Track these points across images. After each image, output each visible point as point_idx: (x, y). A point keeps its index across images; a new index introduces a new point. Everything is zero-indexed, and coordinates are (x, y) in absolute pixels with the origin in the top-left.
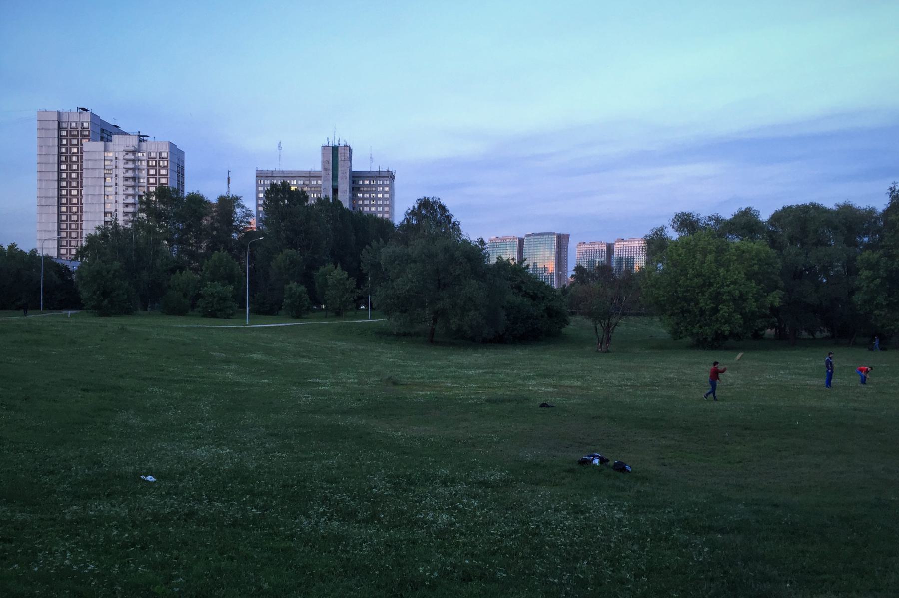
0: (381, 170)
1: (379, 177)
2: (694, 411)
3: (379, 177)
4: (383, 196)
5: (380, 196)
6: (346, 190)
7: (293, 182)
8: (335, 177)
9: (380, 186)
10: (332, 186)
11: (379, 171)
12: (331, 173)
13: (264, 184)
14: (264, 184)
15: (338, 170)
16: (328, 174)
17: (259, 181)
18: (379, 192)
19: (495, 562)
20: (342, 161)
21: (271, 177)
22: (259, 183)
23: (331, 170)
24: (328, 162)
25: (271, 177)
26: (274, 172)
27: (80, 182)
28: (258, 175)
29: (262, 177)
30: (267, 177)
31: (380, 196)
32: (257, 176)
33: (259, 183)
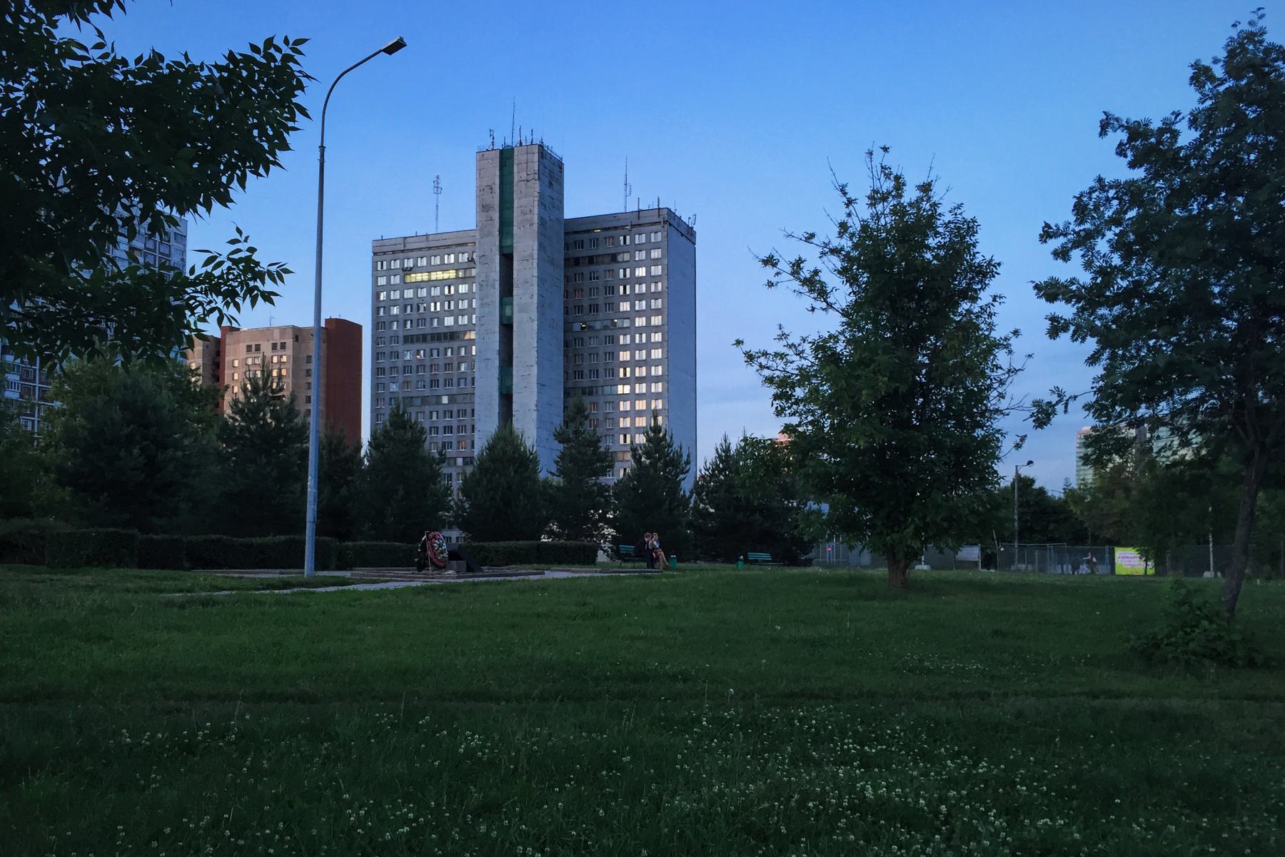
0: (643, 207)
1: (640, 225)
2: (57, 404)
3: (640, 225)
4: (648, 272)
5: (641, 272)
6: (531, 256)
7: (656, 287)
8: (506, 226)
9: (639, 248)
10: (501, 247)
11: (659, 209)
12: (496, 216)
13: (389, 269)
14: (389, 269)
15: (512, 207)
16: (491, 220)
17: (379, 263)
18: (639, 264)
19: (437, 852)
20: (523, 183)
21: (402, 251)
22: (379, 268)
23: (497, 209)
24: (491, 189)
25: (402, 251)
26: (409, 240)
27: (36, 422)
28: (377, 250)
29: (385, 253)
30: (394, 252)
31: (641, 272)
32: (375, 254)
33: (379, 268)
